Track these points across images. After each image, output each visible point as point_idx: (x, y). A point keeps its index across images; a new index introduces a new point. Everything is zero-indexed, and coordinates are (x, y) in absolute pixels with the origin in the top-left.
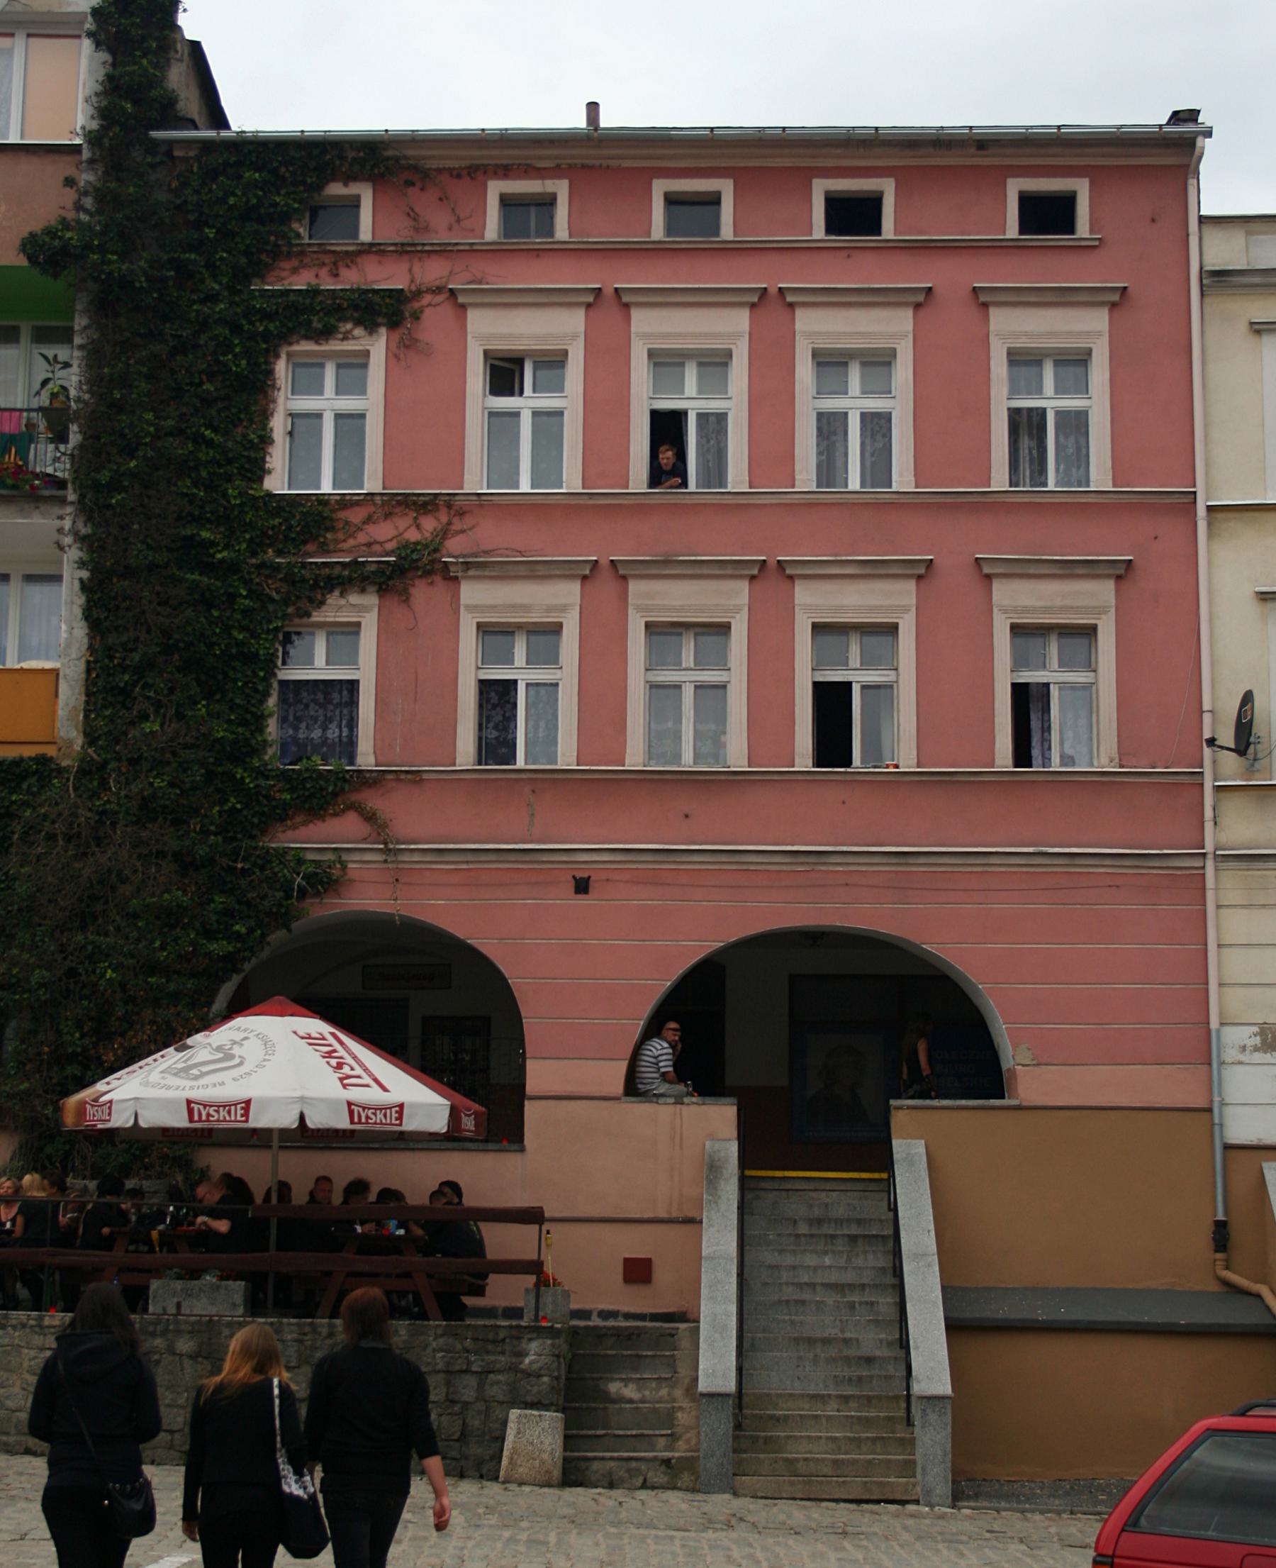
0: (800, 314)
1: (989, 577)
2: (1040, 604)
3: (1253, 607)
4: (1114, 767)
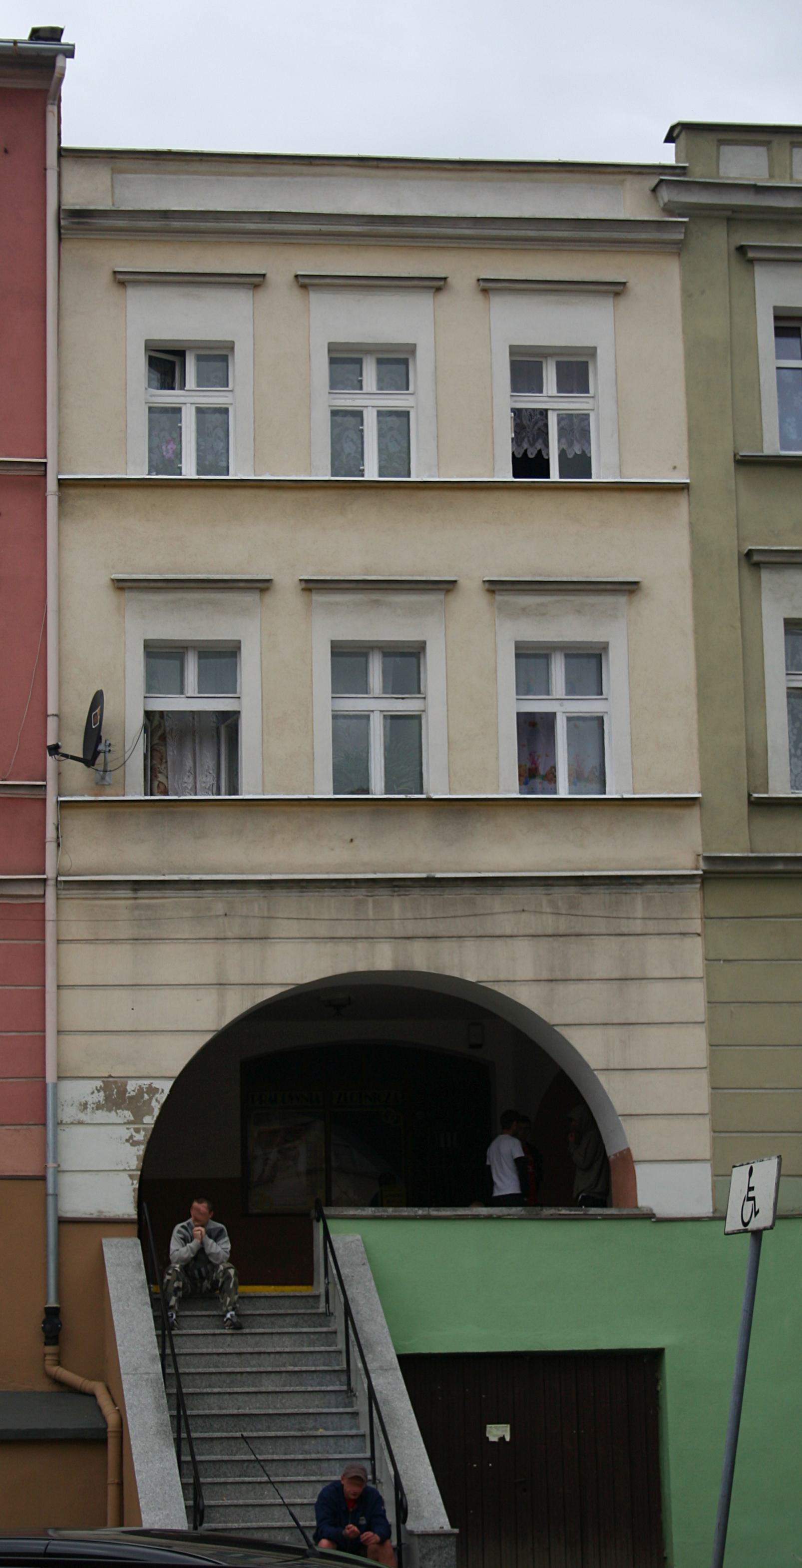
3: (108, 598)
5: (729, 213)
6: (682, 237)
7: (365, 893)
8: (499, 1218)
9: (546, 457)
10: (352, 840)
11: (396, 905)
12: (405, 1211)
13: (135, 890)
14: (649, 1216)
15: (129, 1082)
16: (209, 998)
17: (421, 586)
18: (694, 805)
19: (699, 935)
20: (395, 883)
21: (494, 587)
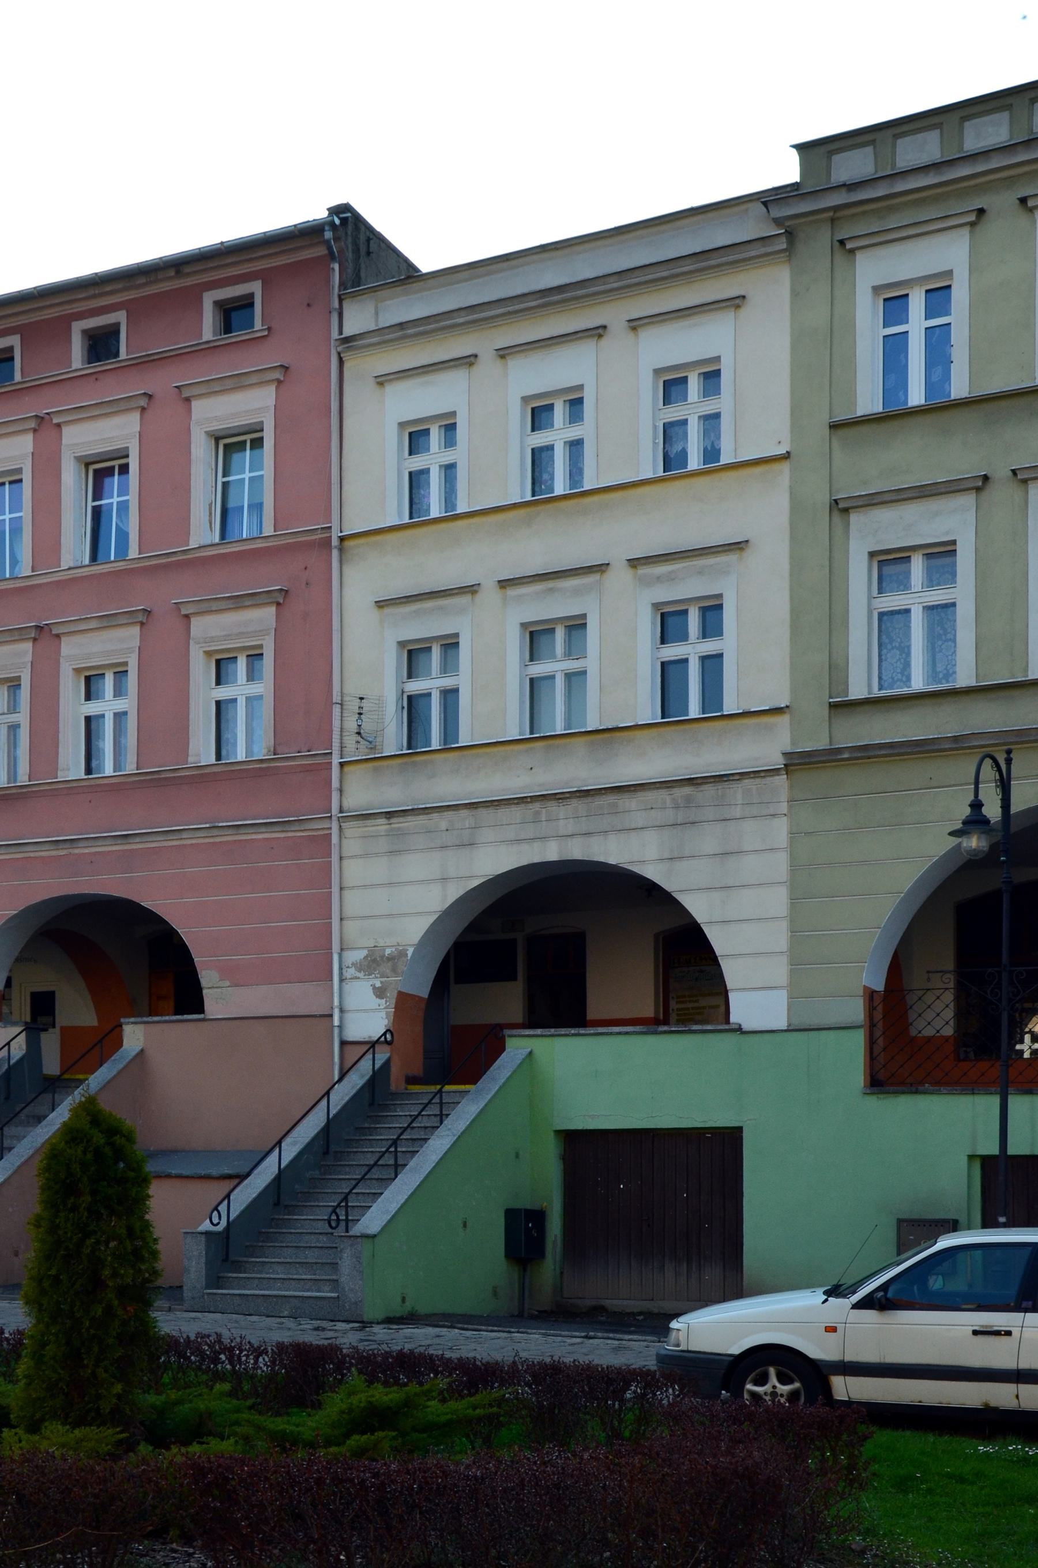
0: (66, 431)
1: (187, 617)
2: (224, 633)
3: (375, 613)
4: (270, 755)
5: (831, 214)
6: (785, 246)
7: (539, 806)
8: (627, 1033)
9: (718, 448)
10: (531, 768)
11: (561, 811)
12: (563, 1031)
13: (389, 818)
14: (739, 1030)
15: (387, 950)
16: (436, 890)
17: (654, 559)
18: (785, 713)
19: (785, 815)
20: (558, 796)
21: (634, 563)
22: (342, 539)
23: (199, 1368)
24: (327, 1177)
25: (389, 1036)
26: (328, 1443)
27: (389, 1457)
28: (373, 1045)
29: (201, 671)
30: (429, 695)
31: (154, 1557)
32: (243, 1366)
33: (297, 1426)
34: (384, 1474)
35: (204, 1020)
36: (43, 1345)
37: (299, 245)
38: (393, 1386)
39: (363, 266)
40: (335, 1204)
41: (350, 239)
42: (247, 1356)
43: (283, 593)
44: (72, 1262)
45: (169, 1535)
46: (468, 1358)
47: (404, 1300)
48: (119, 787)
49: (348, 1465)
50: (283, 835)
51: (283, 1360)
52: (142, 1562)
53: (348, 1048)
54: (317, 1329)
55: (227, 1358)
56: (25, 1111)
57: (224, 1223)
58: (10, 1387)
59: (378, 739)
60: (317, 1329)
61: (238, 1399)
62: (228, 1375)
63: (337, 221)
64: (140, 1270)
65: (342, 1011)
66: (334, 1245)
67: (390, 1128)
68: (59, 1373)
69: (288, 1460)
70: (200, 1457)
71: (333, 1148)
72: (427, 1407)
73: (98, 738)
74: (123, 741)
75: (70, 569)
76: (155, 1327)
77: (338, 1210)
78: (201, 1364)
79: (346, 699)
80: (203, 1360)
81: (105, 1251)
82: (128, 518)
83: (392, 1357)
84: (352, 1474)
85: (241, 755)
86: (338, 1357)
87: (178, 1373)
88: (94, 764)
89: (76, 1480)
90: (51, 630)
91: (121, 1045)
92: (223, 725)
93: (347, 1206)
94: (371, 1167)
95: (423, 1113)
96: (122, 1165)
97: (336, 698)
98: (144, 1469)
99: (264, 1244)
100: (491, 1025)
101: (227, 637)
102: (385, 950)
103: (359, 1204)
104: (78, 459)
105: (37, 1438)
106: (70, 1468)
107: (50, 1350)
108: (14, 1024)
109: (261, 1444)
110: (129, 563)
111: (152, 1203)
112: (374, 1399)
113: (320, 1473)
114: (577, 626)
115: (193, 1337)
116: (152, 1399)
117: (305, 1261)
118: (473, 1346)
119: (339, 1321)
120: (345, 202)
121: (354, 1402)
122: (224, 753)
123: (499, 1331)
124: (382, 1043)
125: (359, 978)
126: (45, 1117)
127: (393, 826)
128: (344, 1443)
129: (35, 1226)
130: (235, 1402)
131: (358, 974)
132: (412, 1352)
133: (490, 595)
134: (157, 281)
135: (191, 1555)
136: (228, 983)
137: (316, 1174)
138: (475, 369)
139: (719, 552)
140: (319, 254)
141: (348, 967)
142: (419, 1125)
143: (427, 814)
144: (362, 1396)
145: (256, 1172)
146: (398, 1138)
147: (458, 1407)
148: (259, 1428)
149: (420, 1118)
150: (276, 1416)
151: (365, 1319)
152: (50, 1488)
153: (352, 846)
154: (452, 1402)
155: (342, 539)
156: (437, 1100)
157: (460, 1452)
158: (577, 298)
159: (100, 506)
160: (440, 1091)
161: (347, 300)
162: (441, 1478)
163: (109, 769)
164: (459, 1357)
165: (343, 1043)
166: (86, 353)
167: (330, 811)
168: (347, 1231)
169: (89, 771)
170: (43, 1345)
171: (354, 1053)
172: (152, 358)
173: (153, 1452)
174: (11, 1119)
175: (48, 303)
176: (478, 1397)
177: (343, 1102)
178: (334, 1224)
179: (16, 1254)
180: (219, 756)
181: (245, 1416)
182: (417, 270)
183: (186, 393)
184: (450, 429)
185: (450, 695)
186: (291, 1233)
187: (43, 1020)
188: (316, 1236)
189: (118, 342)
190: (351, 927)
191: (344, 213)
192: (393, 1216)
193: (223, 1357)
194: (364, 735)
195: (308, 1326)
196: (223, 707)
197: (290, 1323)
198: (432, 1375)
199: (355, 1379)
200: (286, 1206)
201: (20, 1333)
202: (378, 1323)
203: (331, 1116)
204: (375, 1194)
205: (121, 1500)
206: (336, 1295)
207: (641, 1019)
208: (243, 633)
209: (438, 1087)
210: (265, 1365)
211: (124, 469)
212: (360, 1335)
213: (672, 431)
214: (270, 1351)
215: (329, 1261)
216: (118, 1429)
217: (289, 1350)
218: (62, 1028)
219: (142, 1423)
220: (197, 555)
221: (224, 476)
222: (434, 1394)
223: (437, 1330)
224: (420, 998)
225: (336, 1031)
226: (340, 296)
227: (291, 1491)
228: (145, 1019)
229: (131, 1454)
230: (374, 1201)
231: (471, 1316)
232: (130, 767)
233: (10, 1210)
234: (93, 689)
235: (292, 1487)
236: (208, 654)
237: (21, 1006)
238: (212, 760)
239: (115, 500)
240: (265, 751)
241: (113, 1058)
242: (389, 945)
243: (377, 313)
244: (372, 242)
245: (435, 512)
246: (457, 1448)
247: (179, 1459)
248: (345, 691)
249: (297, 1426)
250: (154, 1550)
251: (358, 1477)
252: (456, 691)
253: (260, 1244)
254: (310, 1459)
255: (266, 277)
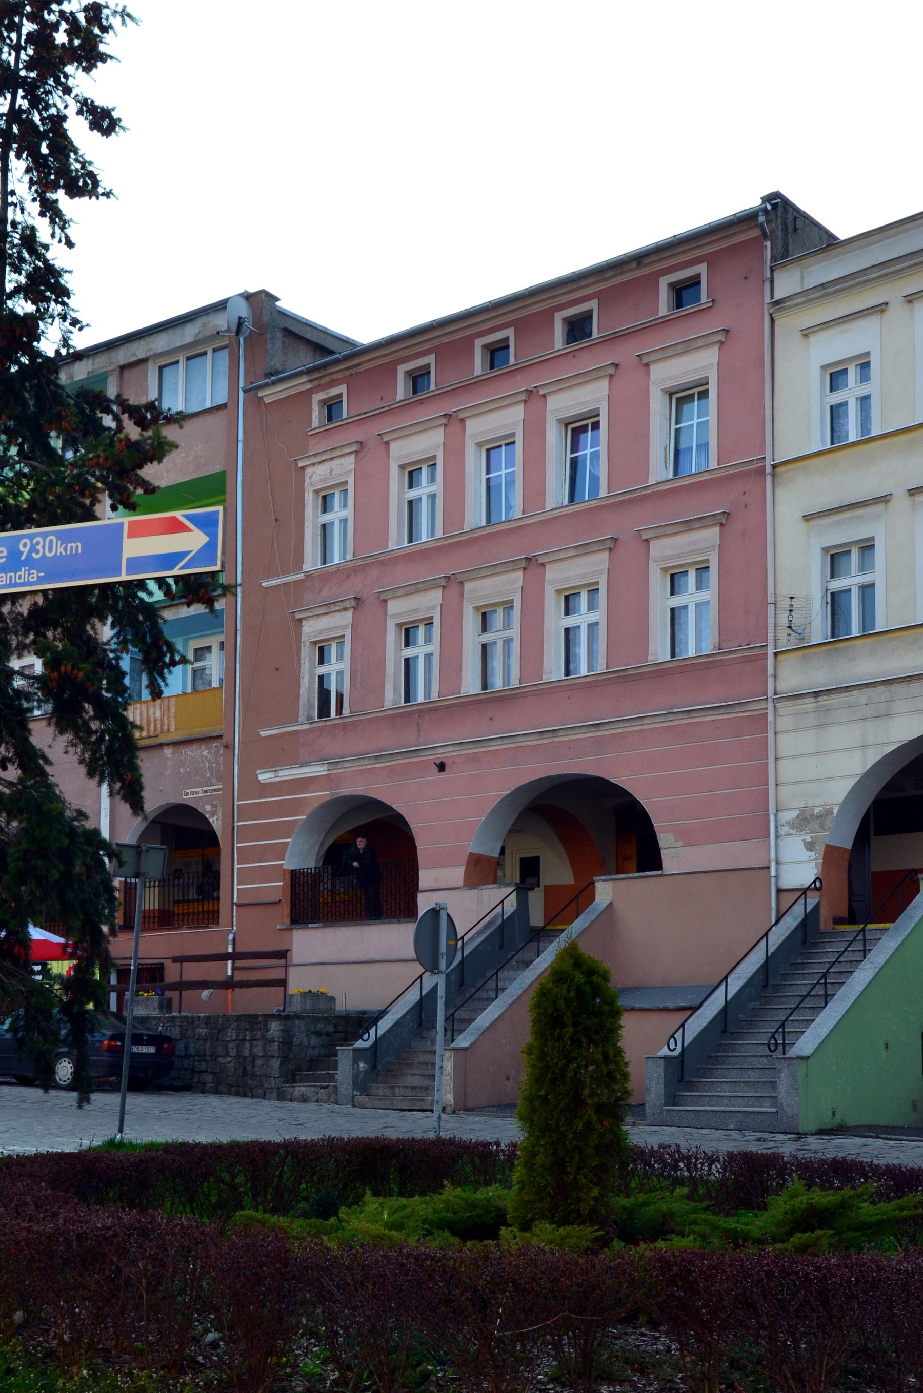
1: (647, 541)
2: (677, 552)
3: (803, 526)
13: (816, 697)
22: (774, 467)
23: (661, 1174)
24: (766, 1007)
25: (818, 884)
26: (775, 1241)
27: (829, 1253)
28: (804, 891)
29: (658, 584)
30: (850, 590)
31: (627, 1340)
32: (699, 1173)
33: (747, 1225)
34: (825, 1268)
35: (661, 875)
36: (534, 1155)
37: (736, 230)
38: (828, 1190)
39: (790, 241)
40: (774, 1030)
41: (780, 221)
42: (702, 1164)
43: (726, 516)
44: (558, 1083)
45: (638, 1320)
46: (894, 1165)
47: (834, 1114)
48: (592, 685)
49: (793, 1259)
50: (726, 717)
51: (733, 1167)
52: (616, 1344)
53: (783, 895)
54: (759, 1140)
55: (685, 1166)
56: (516, 958)
57: (679, 1049)
58: (506, 1191)
59: (806, 631)
60: (759, 1140)
61: (695, 1202)
62: (686, 1180)
63: (769, 207)
64: (613, 1090)
65: (778, 863)
66: (774, 1066)
67: (820, 963)
68: (547, 1179)
69: (742, 1255)
70: (666, 1251)
71: (771, 981)
72: (861, 1208)
73: (575, 645)
74: (595, 647)
75: (552, 510)
76: (626, 1139)
77: (776, 1036)
78: (663, 1171)
79: (779, 599)
80: (665, 1168)
81: (585, 1074)
82: (599, 465)
83: (827, 1164)
84: (797, 1267)
85: (692, 652)
86: (780, 1165)
87: (643, 1179)
88: (572, 667)
89: (563, 1271)
90: (537, 560)
91: (593, 899)
92: (677, 628)
93: (784, 1032)
94: (805, 997)
95: (849, 949)
96: (598, 1000)
97: (770, 599)
98: (620, 1262)
99: (713, 1066)
100: (907, 870)
101: (680, 555)
102: (813, 810)
103: (793, 1030)
104: (664, 391)
105: (528, 1235)
106: (558, 1261)
107: (540, 1159)
108: (507, 885)
109: (716, 1242)
110: (601, 501)
111: (623, 1032)
112: (814, 1201)
113: (769, 1266)
114: (867, 547)
115: (656, 1148)
116: (623, 1201)
117: (748, 1080)
118: (896, 1154)
119: (778, 1133)
120: (775, 190)
121: (796, 1204)
122: (677, 651)
123: (919, 1141)
124: (812, 889)
125: (792, 835)
126: (532, 962)
127: (820, 703)
128: (788, 1240)
129: (527, 1053)
130: (692, 1203)
131: (791, 831)
132: (844, 1159)
133: (901, 502)
134: (622, 273)
135: (657, 1338)
136: (681, 844)
137: (757, 1004)
138: (886, 315)
139: (871, 504)
140: (755, 235)
141: (783, 826)
142: (845, 960)
143: (848, 692)
144: (804, 1199)
145: (706, 1004)
146: (827, 971)
147: (887, 1208)
148: (714, 1227)
149: (846, 953)
150: (727, 1216)
151: (801, 1131)
152: (542, 1278)
153: (785, 723)
154: (882, 1204)
155: (774, 467)
156: (860, 937)
157: (889, 1249)
158: (845, 289)
159: (577, 457)
160: (863, 930)
161: (777, 271)
162: (876, 1272)
163: (583, 670)
164: (886, 1163)
165: (779, 891)
166: (565, 337)
167: (766, 694)
168: (784, 1054)
169: (567, 673)
170: (534, 1155)
171: (788, 899)
172: (618, 335)
173: (625, 1247)
174: (503, 966)
175: (535, 300)
176: (905, 1199)
177: (780, 941)
178: (772, 1048)
179: (508, 1079)
180: (673, 654)
181: (702, 1216)
182: (835, 238)
183: (645, 360)
184: (865, 366)
185: (867, 590)
186: (736, 1056)
187: (529, 881)
188: (758, 1058)
189: (591, 325)
190: (785, 791)
191: (775, 199)
192: (825, 1039)
193: (681, 1165)
194: (794, 628)
195: (751, 1138)
196: (677, 613)
197: (735, 1135)
198: (862, 1180)
199: (795, 1184)
200: (732, 1033)
201: (514, 1145)
202: (812, 1134)
203: (769, 954)
204: (807, 1021)
205: (601, 1290)
206: (775, 1110)
207: (196, 956)
208: (694, 551)
209: (862, 926)
210: (718, 1171)
211: (596, 426)
212: (797, 1145)
213: (836, 413)
214: (722, 1160)
215: (769, 1080)
216: (596, 1228)
217: (738, 1159)
218: (547, 888)
219: (615, 1222)
220: (654, 490)
221: (677, 424)
222: (865, 1197)
223: (863, 1140)
224: (846, 850)
225: (773, 881)
226: (771, 268)
227: (744, 1282)
228: (614, 877)
229: (606, 1250)
230: (807, 1027)
231: (893, 1127)
232: (601, 667)
233: (503, 1041)
234: (571, 605)
235: (745, 1279)
236: (664, 570)
237: (513, 870)
238: (668, 657)
239: (589, 451)
240: (711, 647)
241: (587, 910)
242: (817, 805)
243: (802, 278)
244: (798, 220)
245: (853, 437)
246: (886, 1246)
247: (647, 1253)
248: (778, 593)
249: (747, 1225)
250: (626, 1334)
251: (803, 1269)
252: (872, 586)
253: (710, 1066)
254: (760, 1254)
255: (711, 260)
